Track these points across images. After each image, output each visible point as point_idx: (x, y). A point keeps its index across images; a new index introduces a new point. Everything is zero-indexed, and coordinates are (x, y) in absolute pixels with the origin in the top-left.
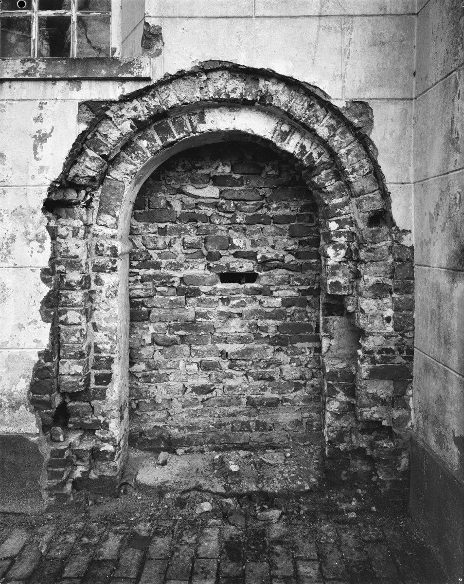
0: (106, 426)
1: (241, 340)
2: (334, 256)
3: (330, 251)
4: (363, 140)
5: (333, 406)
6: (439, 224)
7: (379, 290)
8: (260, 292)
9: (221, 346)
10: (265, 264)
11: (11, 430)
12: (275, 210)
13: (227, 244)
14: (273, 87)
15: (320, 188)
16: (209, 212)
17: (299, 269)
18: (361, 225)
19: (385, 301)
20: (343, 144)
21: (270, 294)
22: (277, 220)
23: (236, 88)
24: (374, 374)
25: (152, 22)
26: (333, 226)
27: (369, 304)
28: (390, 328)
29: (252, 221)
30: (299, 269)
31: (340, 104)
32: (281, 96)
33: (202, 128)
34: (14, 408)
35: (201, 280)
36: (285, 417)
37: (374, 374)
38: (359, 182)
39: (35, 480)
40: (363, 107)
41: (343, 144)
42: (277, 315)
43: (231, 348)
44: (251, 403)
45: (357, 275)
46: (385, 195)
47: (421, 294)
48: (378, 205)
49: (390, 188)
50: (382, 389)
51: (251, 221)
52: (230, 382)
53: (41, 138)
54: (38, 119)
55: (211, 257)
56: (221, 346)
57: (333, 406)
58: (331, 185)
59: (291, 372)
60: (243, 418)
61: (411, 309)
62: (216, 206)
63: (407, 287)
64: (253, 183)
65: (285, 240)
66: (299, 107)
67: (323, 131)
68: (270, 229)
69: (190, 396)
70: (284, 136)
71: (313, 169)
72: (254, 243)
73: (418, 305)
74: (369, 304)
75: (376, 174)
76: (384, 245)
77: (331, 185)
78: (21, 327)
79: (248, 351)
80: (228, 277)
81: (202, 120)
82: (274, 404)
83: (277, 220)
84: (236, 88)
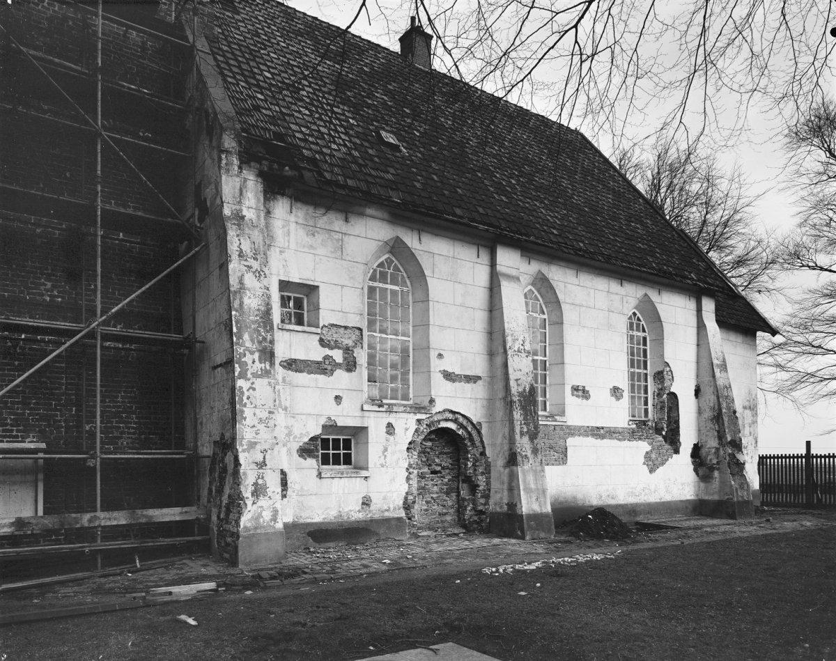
0: (414, 517)
1: (437, 493)
2: (470, 464)
3: (469, 463)
4: (479, 432)
5: (469, 508)
6: (500, 456)
7: (483, 474)
8: (442, 477)
9: (432, 495)
10: (443, 468)
11: (398, 516)
12: (446, 450)
13: (434, 462)
14: (459, 416)
15: (466, 445)
16: (429, 450)
17: (452, 469)
18: (478, 456)
19: (41, 626)
20: (474, 433)
21: (444, 478)
22: (445, 453)
23: (450, 416)
24: (482, 497)
25: (433, 397)
26: (469, 456)
27: (480, 477)
28: (485, 484)
29: (440, 453)
30: (452, 469)
31: (475, 423)
32: (461, 419)
33: (440, 426)
34: (399, 509)
35: (426, 473)
36: (448, 518)
37: (482, 497)
38: (478, 443)
39: (405, 530)
40: (480, 424)
41: (474, 433)
42: (447, 484)
43: (434, 496)
44: (440, 514)
45: (475, 470)
46: (484, 447)
47: (493, 474)
48: (482, 450)
49: (486, 446)
50: (482, 501)
51: (440, 453)
52: (434, 507)
53: (407, 429)
54: (406, 424)
55: (430, 465)
56: (432, 495)
57: (469, 508)
58: (469, 444)
59: (450, 503)
60: (437, 519)
61: (490, 478)
62: (431, 448)
63: (489, 473)
64: (441, 441)
65: (450, 460)
66: (465, 423)
67: (470, 429)
68: (445, 456)
69: (423, 512)
70: (458, 429)
71: (464, 439)
72: (441, 461)
73: (492, 477)
74: (480, 477)
75: (482, 442)
76: (483, 461)
77: (469, 444)
78: (401, 485)
79: (439, 496)
80: (433, 472)
81: (439, 424)
82: (446, 514)
83: (445, 453)
84: (450, 416)
